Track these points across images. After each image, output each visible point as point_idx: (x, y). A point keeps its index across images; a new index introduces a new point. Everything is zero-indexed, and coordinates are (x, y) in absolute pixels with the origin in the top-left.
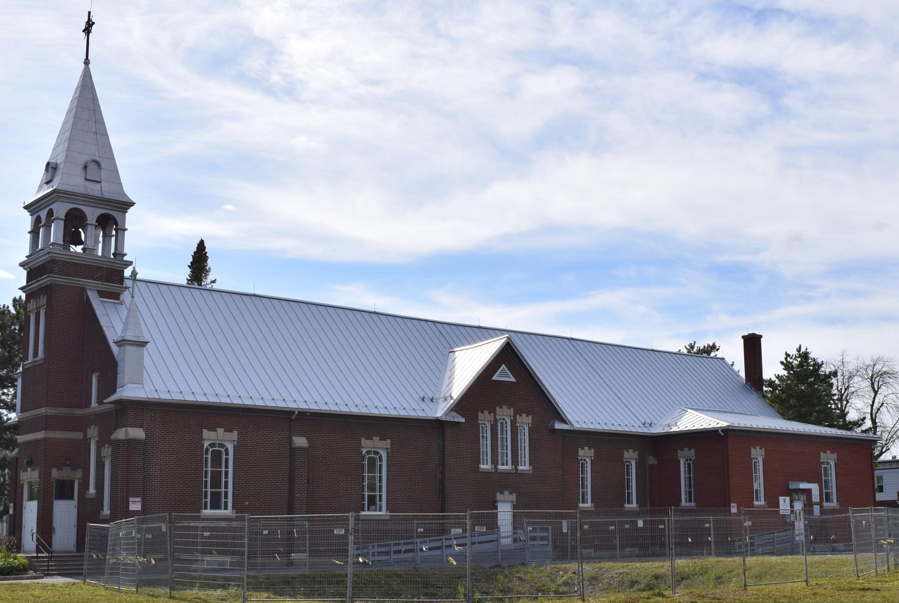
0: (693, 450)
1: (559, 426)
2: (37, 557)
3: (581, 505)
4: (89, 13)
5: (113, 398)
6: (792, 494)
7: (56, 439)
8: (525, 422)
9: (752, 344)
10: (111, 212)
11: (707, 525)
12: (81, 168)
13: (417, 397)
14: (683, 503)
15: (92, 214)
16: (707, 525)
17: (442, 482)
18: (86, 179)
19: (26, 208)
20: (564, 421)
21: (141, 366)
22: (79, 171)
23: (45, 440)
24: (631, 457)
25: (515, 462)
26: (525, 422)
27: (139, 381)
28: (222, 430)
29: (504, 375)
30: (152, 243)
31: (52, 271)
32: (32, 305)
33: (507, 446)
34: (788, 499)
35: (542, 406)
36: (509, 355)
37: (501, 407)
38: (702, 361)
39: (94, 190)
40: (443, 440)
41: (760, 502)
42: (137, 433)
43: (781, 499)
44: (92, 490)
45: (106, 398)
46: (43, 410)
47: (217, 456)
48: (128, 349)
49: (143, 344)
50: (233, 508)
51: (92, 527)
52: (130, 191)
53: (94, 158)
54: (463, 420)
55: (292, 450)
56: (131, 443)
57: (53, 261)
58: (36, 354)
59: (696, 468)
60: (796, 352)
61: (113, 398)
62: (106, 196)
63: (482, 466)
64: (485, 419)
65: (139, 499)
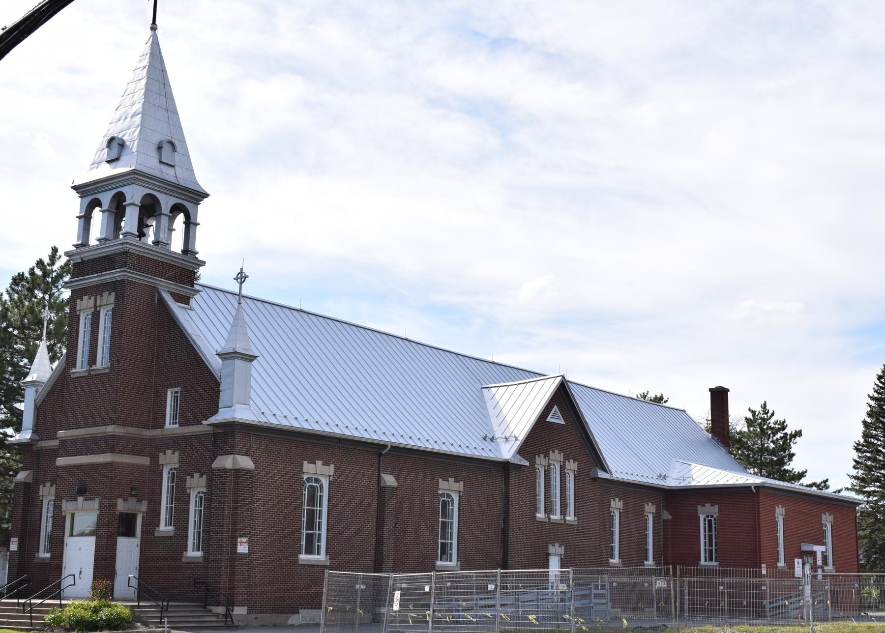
0: (716, 506)
1: (602, 475)
2: (138, 607)
3: (303, 557)
6: (802, 554)
7: (123, 464)
8: (572, 466)
9: (719, 397)
10: (185, 203)
11: (615, 584)
12: (155, 147)
13: (480, 437)
14: (702, 562)
15: (166, 202)
16: (615, 584)
17: (505, 532)
18: (161, 162)
19: (75, 188)
20: (604, 469)
21: (247, 386)
22: (154, 153)
23: (111, 464)
24: (650, 509)
25: (563, 512)
26: (572, 466)
27: (246, 402)
28: (321, 462)
29: (556, 418)
30: (222, 240)
31: (125, 265)
32: (85, 304)
33: (543, 493)
34: (800, 560)
35: (589, 454)
36: (563, 396)
38: (655, 408)
39: (168, 174)
40: (507, 483)
41: (781, 564)
42: (245, 462)
43: (796, 560)
44: (164, 528)
46: (110, 429)
47: (312, 490)
48: (238, 363)
49: (251, 358)
50: (327, 553)
51: (330, 575)
52: (203, 179)
53: (173, 140)
54: (528, 464)
55: (382, 490)
56: (238, 472)
57: (126, 253)
58: (92, 360)
59: (719, 526)
60: (760, 409)
62: (182, 183)
63: (538, 515)
64: (541, 461)
65: (246, 540)
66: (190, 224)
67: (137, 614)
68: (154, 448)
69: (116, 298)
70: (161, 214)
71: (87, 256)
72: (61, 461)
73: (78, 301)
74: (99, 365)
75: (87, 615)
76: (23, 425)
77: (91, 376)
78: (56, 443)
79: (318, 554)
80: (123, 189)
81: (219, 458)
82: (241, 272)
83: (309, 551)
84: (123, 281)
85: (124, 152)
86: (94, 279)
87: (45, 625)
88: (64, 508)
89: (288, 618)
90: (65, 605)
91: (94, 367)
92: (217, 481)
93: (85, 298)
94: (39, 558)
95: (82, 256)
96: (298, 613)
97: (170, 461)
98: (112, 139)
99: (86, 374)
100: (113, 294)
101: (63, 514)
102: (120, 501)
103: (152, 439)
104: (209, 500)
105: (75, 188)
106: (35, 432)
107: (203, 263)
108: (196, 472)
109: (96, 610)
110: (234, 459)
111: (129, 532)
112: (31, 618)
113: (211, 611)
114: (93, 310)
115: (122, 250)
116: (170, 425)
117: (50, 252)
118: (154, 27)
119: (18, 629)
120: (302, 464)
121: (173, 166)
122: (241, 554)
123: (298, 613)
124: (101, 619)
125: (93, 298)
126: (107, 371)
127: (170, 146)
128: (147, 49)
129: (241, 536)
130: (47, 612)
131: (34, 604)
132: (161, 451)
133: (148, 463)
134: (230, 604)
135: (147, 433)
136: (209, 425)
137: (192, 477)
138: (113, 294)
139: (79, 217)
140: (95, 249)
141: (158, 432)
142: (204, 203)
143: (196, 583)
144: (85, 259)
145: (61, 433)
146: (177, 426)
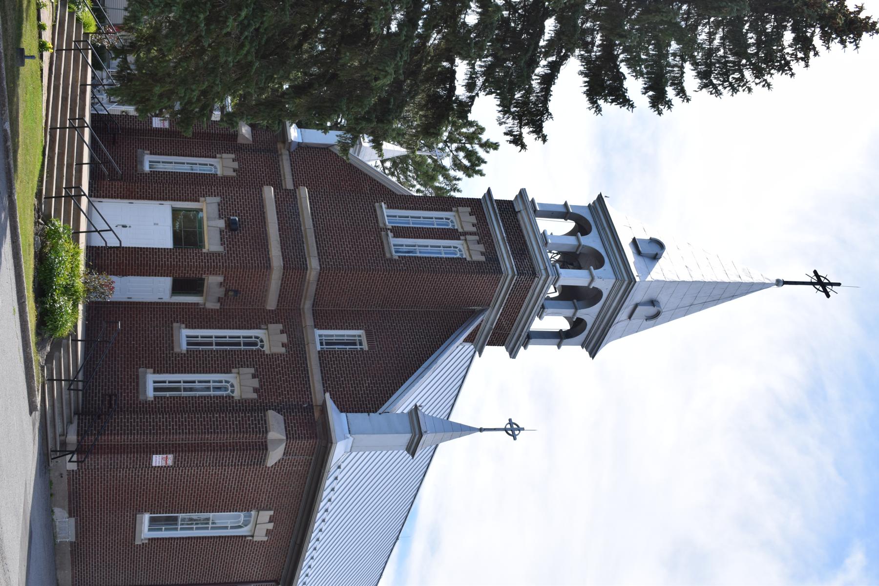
2: (75, 340)
4: (839, 284)
5: (331, 405)
15: (589, 314)
18: (636, 306)
19: (600, 198)
22: (646, 298)
23: (268, 267)
31: (520, 273)
32: (465, 221)
37: (254, 376)
42: (275, 456)
44: (184, 335)
45: (332, 397)
46: (314, 264)
48: (406, 438)
56: (263, 448)
58: (399, 232)
61: (331, 405)
65: (170, 462)
66: (559, 337)
67: (64, 341)
68: (287, 316)
69: (479, 263)
70: (576, 309)
71: (523, 218)
72: (269, 192)
73: (469, 209)
74: (394, 241)
75: (61, 281)
76: (307, 130)
77: (378, 231)
78: (289, 184)
79: (149, 530)
80: (607, 265)
81: (280, 418)
82: (520, 429)
83: (152, 520)
84: (500, 272)
85: (647, 260)
86: (498, 232)
87: (47, 219)
88: (209, 199)
89: (63, 507)
90: (76, 240)
91: (390, 234)
92: (251, 413)
93: (473, 219)
94: (143, 156)
95: (524, 213)
96: (70, 516)
97: (270, 339)
98: (661, 245)
99: (381, 225)
100: (483, 258)
101: (202, 199)
102: (220, 279)
103: (299, 312)
104: (224, 406)
105: (600, 198)
106: (301, 146)
107: (513, 354)
108: (260, 381)
109: (69, 290)
110: (281, 441)
111: (178, 287)
112: (58, 197)
113: (70, 422)
114: (460, 230)
115: (537, 269)
116: (318, 337)
117: (493, 140)
118: (780, 283)
119: (42, 170)
120: (270, 509)
121: (630, 317)
122: (151, 459)
123: (70, 516)
124: (55, 301)
125: (474, 229)
126: (388, 255)
127: (655, 311)
128: (757, 279)
129: (175, 458)
130: (67, 221)
131: (79, 201)
132: (284, 326)
133: (268, 308)
134: (82, 450)
135: (307, 306)
136: (325, 402)
137: (254, 376)
138: (483, 258)
139: (566, 204)
140: (534, 227)
141: (309, 320)
142: (585, 353)
143: (110, 396)
144: (519, 215)
145: (304, 192)
146: (319, 348)
